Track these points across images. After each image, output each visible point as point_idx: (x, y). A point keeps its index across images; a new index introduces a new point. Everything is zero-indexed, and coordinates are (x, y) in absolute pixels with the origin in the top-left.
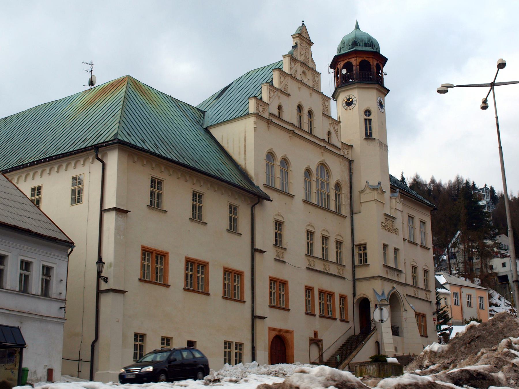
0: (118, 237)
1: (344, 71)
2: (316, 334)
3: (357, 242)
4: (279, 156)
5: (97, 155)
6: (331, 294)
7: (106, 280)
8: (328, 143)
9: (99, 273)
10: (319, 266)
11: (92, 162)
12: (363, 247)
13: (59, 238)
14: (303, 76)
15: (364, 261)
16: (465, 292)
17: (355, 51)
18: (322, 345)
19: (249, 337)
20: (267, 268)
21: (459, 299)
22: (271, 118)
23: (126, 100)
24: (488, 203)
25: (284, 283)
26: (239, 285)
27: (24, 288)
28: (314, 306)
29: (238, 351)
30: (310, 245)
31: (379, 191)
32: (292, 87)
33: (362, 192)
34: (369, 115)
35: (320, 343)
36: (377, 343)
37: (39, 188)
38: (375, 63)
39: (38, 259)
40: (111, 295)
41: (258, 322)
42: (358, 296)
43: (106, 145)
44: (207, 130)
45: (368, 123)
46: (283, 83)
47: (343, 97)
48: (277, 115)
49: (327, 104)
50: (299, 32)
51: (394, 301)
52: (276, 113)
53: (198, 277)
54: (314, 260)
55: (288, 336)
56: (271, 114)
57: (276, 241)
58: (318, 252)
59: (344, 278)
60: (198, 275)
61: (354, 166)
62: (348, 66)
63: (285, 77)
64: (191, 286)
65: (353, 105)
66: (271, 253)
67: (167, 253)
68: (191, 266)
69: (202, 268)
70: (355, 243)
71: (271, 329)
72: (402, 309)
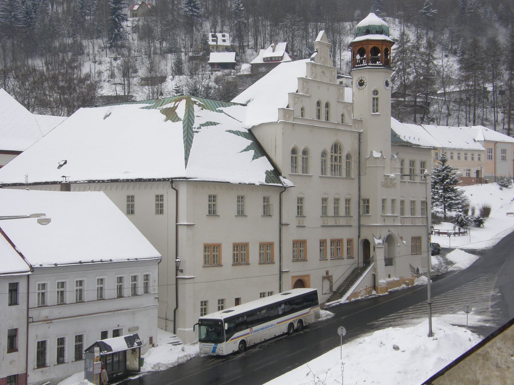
2: (327, 273)
15: (367, 209)
18: (332, 279)
21: (493, 154)
28: (326, 253)
30: (324, 209)
34: (377, 94)
35: (330, 278)
47: (356, 77)
57: (298, 212)
58: (331, 212)
59: (351, 226)
64: (237, 261)
65: (364, 86)
67: (221, 244)
69: (245, 247)
71: (293, 277)
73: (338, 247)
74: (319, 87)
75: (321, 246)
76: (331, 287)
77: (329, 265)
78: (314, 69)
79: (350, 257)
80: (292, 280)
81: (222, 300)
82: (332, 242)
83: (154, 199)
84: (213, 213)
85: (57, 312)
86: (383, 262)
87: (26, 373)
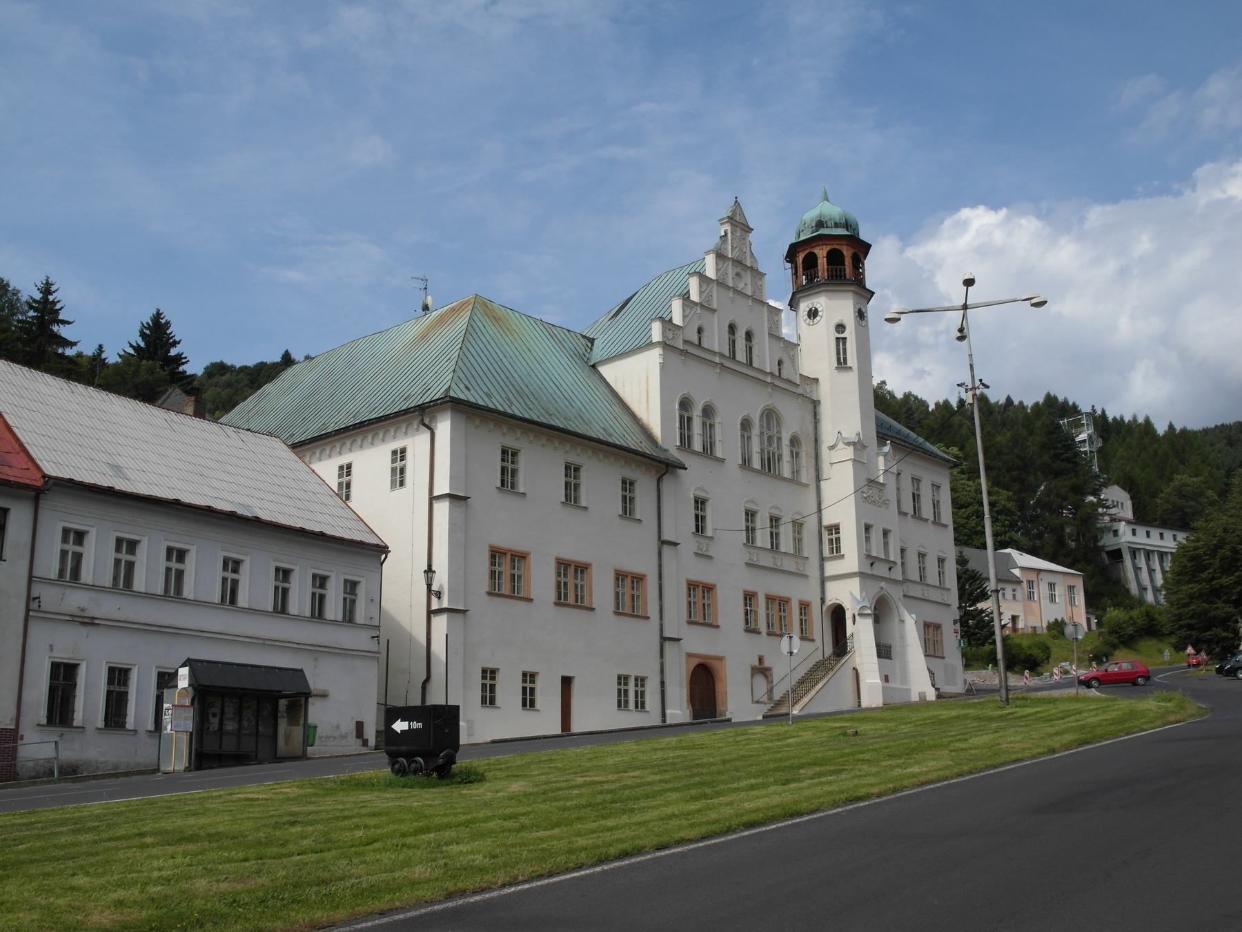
2: (761, 659)
6: (783, 602)
10: (766, 560)
13: (337, 535)
25: (709, 589)
30: (750, 531)
33: (832, 448)
42: (829, 602)
45: (841, 342)
55: (716, 665)
58: (763, 538)
66: (689, 543)
71: (689, 655)
72: (896, 620)
76: (770, 691)
77: (762, 645)
78: (721, 264)
80: (687, 663)
81: (533, 675)
82: (770, 599)
83: (388, 457)
84: (513, 487)
85: (109, 606)
87: (16, 730)
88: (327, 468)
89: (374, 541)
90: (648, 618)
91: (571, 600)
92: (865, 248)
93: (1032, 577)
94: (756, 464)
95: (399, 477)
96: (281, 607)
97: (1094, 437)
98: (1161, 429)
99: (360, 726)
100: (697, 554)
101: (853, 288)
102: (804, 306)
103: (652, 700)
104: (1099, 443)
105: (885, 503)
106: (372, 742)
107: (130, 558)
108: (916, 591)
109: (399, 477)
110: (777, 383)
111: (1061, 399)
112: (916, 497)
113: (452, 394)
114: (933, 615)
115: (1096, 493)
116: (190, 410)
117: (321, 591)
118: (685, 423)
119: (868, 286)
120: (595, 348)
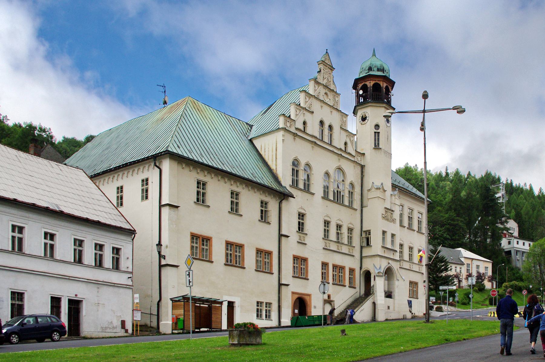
0: (172, 226)
1: (361, 92)
3: (364, 229)
4: (303, 162)
5: (155, 163)
6: (342, 268)
7: (164, 257)
8: (345, 151)
9: (159, 253)
10: (333, 247)
11: (154, 168)
12: (368, 232)
13: (124, 227)
14: (325, 96)
16: (475, 263)
17: (370, 75)
19: (277, 299)
20: (291, 248)
21: (470, 268)
22: (296, 132)
23: (182, 118)
24: (503, 195)
25: (305, 260)
26: (269, 261)
27: (99, 263)
29: (268, 309)
30: (326, 232)
31: (381, 190)
32: (316, 106)
33: (369, 190)
34: (378, 129)
35: (332, 303)
36: (374, 304)
37: (122, 187)
38: (385, 85)
39: (109, 241)
40: (169, 268)
41: (283, 288)
42: (363, 270)
43: (160, 155)
44: (251, 141)
45: (377, 134)
46: (308, 103)
48: (303, 130)
49: (344, 119)
50: (323, 59)
51: (389, 273)
52: (301, 127)
53: (236, 256)
54: (330, 242)
55: (307, 298)
56: (297, 129)
58: (333, 236)
59: (353, 256)
60: (236, 254)
61: (366, 170)
62: (365, 88)
63: (310, 98)
65: (367, 118)
66: (294, 237)
68: (231, 247)
70: (363, 230)
71: (293, 293)
72: (395, 279)
73: (341, 274)
74: (322, 106)
75: (322, 269)
77: (331, 289)
79: (352, 286)
82: (335, 266)
83: (140, 183)
86: (383, 294)
88: (110, 187)
89: (127, 226)
90: (273, 274)
91: (234, 262)
92: (392, 83)
93: (469, 262)
94: (331, 197)
95: (145, 195)
96: (79, 260)
97: (505, 195)
98: (536, 192)
99: (123, 323)
100: (298, 242)
101: (384, 105)
102: (360, 113)
103: (274, 315)
104: (506, 199)
105: (393, 221)
106: (130, 331)
107: (20, 236)
108: (406, 265)
109: (145, 195)
110: (343, 154)
111: (493, 174)
112: (410, 219)
113: (170, 149)
114: (416, 278)
115: (502, 223)
116: (32, 151)
117: (80, 248)
118: (295, 173)
119: (392, 105)
120: (252, 130)
